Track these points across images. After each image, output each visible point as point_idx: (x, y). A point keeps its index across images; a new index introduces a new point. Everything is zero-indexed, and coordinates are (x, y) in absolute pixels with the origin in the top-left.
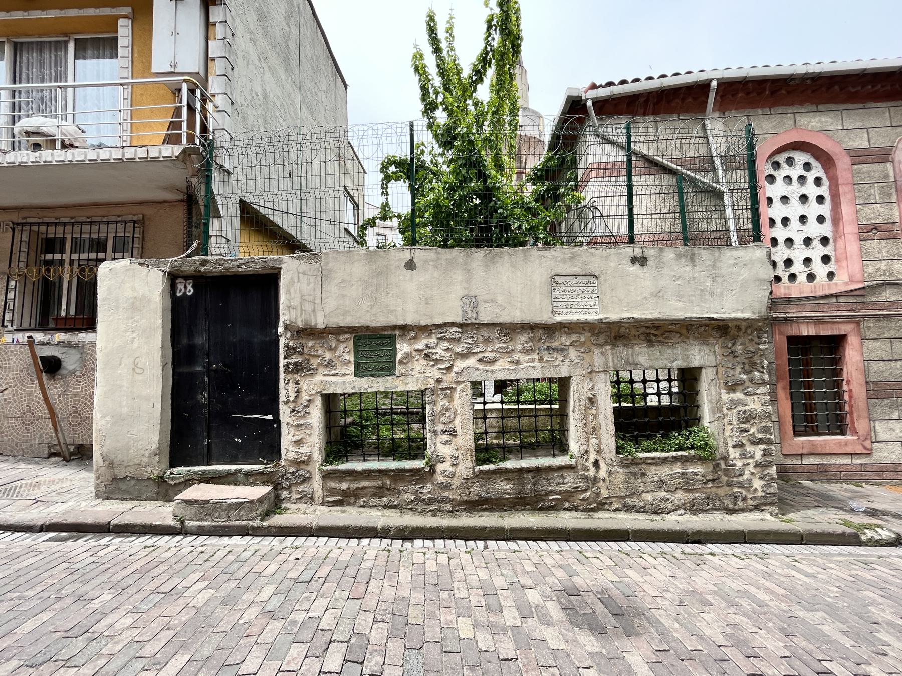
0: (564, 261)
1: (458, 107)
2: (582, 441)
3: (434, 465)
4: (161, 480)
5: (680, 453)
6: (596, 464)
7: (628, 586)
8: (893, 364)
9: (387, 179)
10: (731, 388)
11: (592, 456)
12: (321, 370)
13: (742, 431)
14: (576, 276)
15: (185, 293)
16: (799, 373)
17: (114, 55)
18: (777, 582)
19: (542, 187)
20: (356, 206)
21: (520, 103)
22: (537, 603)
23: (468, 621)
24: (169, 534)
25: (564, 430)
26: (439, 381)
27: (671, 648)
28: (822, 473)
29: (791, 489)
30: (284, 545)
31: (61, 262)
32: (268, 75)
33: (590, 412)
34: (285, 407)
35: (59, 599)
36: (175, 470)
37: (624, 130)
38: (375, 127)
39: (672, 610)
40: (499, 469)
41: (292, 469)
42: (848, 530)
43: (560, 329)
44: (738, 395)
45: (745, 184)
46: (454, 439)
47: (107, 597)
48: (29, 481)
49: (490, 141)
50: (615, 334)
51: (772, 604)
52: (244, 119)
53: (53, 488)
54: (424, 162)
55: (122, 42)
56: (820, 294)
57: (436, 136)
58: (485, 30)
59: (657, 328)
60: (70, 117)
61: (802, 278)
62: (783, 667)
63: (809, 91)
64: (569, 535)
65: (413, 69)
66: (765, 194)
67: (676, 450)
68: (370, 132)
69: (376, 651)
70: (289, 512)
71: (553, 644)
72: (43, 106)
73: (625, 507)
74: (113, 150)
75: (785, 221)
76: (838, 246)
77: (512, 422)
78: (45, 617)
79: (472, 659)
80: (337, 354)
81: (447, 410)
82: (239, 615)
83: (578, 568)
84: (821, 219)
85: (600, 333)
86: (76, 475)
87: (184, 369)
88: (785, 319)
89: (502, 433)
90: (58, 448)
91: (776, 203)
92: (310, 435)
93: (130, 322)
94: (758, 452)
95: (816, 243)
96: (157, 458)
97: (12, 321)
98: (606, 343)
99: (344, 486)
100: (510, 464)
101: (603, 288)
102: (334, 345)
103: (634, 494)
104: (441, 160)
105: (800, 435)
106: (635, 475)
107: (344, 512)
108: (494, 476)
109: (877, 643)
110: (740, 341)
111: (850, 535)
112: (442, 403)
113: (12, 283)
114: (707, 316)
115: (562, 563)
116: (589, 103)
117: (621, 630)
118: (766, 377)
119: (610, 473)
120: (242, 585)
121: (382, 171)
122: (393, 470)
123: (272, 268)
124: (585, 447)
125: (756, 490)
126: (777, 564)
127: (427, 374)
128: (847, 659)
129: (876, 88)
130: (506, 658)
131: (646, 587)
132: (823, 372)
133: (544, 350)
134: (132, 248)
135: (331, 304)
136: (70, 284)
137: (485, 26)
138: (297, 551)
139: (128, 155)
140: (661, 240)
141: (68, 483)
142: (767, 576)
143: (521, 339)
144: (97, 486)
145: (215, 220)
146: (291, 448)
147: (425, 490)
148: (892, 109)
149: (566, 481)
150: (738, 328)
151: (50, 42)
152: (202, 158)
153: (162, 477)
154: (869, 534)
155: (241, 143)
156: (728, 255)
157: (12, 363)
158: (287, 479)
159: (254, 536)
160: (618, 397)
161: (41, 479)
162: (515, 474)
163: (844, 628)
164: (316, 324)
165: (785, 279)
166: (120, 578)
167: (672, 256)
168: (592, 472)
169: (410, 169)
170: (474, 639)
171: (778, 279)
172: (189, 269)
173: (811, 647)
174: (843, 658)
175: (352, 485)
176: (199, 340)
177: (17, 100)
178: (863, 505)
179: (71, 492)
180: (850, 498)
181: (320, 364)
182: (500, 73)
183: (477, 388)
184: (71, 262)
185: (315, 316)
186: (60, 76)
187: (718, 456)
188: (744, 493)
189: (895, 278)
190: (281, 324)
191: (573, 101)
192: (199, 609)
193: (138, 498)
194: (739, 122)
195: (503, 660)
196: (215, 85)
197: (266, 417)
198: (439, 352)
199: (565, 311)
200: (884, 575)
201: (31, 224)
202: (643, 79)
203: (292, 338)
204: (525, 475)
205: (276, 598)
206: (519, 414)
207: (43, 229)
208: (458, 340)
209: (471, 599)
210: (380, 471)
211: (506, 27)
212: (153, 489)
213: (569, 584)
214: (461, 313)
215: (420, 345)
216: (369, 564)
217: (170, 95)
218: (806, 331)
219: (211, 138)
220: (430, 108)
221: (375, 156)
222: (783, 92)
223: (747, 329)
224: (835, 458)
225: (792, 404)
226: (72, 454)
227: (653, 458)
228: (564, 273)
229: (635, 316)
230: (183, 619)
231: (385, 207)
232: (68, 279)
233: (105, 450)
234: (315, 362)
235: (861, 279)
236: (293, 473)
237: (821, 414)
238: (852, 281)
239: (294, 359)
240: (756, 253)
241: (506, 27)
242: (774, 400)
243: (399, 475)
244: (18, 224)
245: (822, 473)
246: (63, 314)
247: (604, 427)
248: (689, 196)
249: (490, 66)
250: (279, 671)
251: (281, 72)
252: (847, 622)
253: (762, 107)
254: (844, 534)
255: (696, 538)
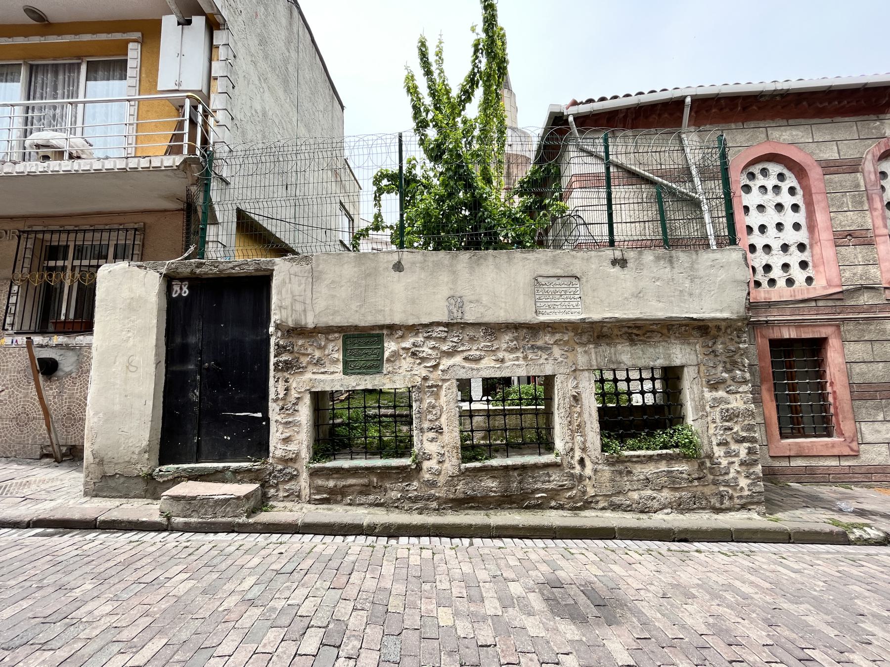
0: (546, 263)
1: (447, 124)
2: (567, 439)
3: (420, 463)
4: (149, 478)
5: (664, 451)
6: (582, 462)
7: (612, 579)
8: (875, 366)
9: (380, 191)
10: (714, 386)
11: (578, 454)
12: (310, 368)
13: (725, 429)
14: (559, 277)
15: (180, 294)
16: (783, 376)
17: (123, 77)
18: (763, 577)
19: (529, 200)
20: (351, 219)
21: (507, 122)
22: (519, 594)
23: (449, 611)
24: (155, 531)
25: (550, 428)
26: (425, 379)
27: (653, 636)
28: (811, 475)
29: (779, 491)
30: (269, 541)
31: (64, 268)
32: (267, 95)
33: (575, 410)
34: (274, 405)
35: (40, 588)
36: (164, 468)
37: (602, 141)
38: (365, 139)
39: (655, 601)
40: (485, 467)
41: (280, 467)
42: (836, 529)
43: (544, 328)
44: (721, 394)
45: (720, 192)
46: (440, 437)
47: (88, 586)
48: (20, 481)
49: (478, 156)
50: (597, 333)
51: (756, 596)
52: (244, 133)
53: (43, 487)
54: (415, 176)
55: (131, 63)
56: (800, 297)
57: (426, 151)
58: (472, 53)
59: (638, 327)
60: (79, 131)
61: (781, 283)
62: (764, 654)
63: (779, 107)
64: (555, 533)
65: (405, 90)
66: (741, 202)
67: (661, 449)
68: (361, 143)
69: (354, 636)
70: (275, 509)
71: (533, 632)
72: (54, 122)
73: (611, 505)
74: (118, 161)
75: (763, 228)
76: (815, 252)
77: (499, 422)
78: (25, 604)
79: (451, 645)
80: (326, 352)
81: (434, 407)
82: (218, 603)
83: (562, 563)
84: (797, 226)
85: (583, 333)
86: (66, 475)
87: (177, 368)
88: (767, 322)
89: (489, 431)
90: (50, 449)
91: (753, 211)
92: (298, 433)
93: (127, 321)
94: (742, 450)
95: (793, 249)
96: (146, 456)
97: (12, 325)
98: (589, 342)
99: (331, 484)
100: (495, 462)
101: (585, 288)
102: (323, 343)
103: (619, 493)
104: (431, 174)
105: (787, 438)
106: (620, 473)
107: (330, 509)
108: (480, 474)
109: (861, 633)
110: (720, 340)
111: (838, 534)
112: (428, 401)
113: (15, 288)
114: (687, 316)
115: (546, 558)
116: (571, 119)
117: (602, 619)
118: (748, 376)
119: (596, 472)
120: (224, 576)
121: (375, 184)
122: (379, 468)
123: (265, 270)
124: (570, 445)
125: (742, 489)
126: (764, 560)
127: (413, 372)
128: (831, 647)
129: (842, 104)
130: (484, 643)
131: (630, 580)
132: (806, 375)
133: (529, 349)
134: (132, 254)
135: (321, 305)
136: (71, 288)
137: (473, 49)
138: (282, 546)
139: (131, 165)
140: (642, 245)
141: (59, 482)
142: (753, 571)
143: (506, 339)
144: (86, 484)
145: (212, 227)
146: (279, 446)
147: (411, 488)
148: (859, 123)
149: (552, 479)
150: (718, 328)
151: (64, 64)
152: (202, 168)
153: (151, 475)
154: (858, 533)
155: (239, 153)
156: (705, 258)
157: (8, 377)
158: (275, 477)
159: (239, 533)
160: (602, 396)
161: (33, 478)
162: (501, 472)
163: (829, 618)
164: (306, 324)
165: (765, 284)
166: (103, 570)
167: (651, 258)
168: (578, 470)
169: (402, 182)
170: (454, 626)
171: (758, 284)
172: (185, 271)
173: (794, 636)
174: (825, 646)
175: (339, 483)
176: (193, 340)
177: (30, 114)
178: (853, 505)
179: (62, 490)
180: (839, 499)
181: (309, 363)
182: (487, 92)
183: (464, 386)
184: (73, 268)
185: (305, 315)
186: (74, 94)
187: (703, 455)
188: (730, 492)
189: (871, 282)
190: (272, 324)
191: (556, 117)
192: (179, 598)
193: (126, 496)
194: (712, 134)
195: (481, 646)
196: (216, 102)
197: (255, 415)
198: (426, 350)
199: (548, 311)
200: (872, 571)
201: (36, 232)
202: (621, 96)
203: (283, 337)
204: (511, 473)
205: (256, 588)
206: (504, 413)
207: (47, 236)
208: (444, 339)
209: (453, 590)
210: (367, 469)
211: (492, 47)
212: (142, 486)
213: (552, 576)
214: (447, 312)
215: (407, 344)
216: (350, 558)
217: (175, 112)
218: (788, 333)
219: (211, 149)
220: (422, 125)
221: (366, 165)
222: (755, 107)
223: (726, 328)
224: (823, 459)
225: (778, 406)
226: (64, 455)
227: (638, 456)
228: (546, 274)
229: (617, 315)
230: (163, 606)
231: (378, 216)
232: (69, 283)
233: (96, 447)
234: (304, 360)
235: (838, 283)
236: (280, 471)
237: (807, 416)
238: (829, 285)
239: (285, 357)
240: (733, 255)
241: (492, 47)
242: (757, 401)
243: (385, 473)
244: (24, 232)
245: (811, 475)
246: (63, 318)
247: (588, 425)
248: (669, 204)
249: (477, 86)
250: (254, 653)
251: (280, 93)
252: (832, 613)
253: (735, 122)
254: (831, 533)
255: (683, 536)
